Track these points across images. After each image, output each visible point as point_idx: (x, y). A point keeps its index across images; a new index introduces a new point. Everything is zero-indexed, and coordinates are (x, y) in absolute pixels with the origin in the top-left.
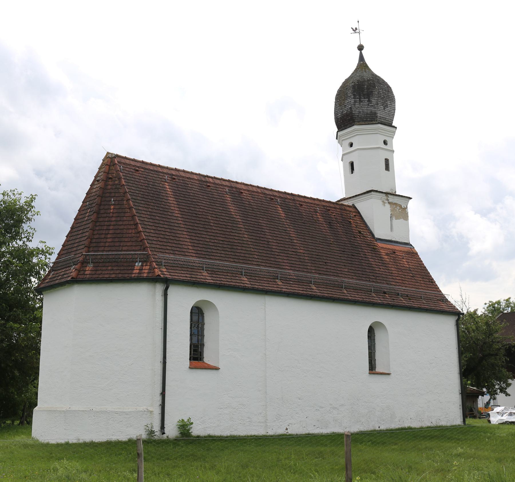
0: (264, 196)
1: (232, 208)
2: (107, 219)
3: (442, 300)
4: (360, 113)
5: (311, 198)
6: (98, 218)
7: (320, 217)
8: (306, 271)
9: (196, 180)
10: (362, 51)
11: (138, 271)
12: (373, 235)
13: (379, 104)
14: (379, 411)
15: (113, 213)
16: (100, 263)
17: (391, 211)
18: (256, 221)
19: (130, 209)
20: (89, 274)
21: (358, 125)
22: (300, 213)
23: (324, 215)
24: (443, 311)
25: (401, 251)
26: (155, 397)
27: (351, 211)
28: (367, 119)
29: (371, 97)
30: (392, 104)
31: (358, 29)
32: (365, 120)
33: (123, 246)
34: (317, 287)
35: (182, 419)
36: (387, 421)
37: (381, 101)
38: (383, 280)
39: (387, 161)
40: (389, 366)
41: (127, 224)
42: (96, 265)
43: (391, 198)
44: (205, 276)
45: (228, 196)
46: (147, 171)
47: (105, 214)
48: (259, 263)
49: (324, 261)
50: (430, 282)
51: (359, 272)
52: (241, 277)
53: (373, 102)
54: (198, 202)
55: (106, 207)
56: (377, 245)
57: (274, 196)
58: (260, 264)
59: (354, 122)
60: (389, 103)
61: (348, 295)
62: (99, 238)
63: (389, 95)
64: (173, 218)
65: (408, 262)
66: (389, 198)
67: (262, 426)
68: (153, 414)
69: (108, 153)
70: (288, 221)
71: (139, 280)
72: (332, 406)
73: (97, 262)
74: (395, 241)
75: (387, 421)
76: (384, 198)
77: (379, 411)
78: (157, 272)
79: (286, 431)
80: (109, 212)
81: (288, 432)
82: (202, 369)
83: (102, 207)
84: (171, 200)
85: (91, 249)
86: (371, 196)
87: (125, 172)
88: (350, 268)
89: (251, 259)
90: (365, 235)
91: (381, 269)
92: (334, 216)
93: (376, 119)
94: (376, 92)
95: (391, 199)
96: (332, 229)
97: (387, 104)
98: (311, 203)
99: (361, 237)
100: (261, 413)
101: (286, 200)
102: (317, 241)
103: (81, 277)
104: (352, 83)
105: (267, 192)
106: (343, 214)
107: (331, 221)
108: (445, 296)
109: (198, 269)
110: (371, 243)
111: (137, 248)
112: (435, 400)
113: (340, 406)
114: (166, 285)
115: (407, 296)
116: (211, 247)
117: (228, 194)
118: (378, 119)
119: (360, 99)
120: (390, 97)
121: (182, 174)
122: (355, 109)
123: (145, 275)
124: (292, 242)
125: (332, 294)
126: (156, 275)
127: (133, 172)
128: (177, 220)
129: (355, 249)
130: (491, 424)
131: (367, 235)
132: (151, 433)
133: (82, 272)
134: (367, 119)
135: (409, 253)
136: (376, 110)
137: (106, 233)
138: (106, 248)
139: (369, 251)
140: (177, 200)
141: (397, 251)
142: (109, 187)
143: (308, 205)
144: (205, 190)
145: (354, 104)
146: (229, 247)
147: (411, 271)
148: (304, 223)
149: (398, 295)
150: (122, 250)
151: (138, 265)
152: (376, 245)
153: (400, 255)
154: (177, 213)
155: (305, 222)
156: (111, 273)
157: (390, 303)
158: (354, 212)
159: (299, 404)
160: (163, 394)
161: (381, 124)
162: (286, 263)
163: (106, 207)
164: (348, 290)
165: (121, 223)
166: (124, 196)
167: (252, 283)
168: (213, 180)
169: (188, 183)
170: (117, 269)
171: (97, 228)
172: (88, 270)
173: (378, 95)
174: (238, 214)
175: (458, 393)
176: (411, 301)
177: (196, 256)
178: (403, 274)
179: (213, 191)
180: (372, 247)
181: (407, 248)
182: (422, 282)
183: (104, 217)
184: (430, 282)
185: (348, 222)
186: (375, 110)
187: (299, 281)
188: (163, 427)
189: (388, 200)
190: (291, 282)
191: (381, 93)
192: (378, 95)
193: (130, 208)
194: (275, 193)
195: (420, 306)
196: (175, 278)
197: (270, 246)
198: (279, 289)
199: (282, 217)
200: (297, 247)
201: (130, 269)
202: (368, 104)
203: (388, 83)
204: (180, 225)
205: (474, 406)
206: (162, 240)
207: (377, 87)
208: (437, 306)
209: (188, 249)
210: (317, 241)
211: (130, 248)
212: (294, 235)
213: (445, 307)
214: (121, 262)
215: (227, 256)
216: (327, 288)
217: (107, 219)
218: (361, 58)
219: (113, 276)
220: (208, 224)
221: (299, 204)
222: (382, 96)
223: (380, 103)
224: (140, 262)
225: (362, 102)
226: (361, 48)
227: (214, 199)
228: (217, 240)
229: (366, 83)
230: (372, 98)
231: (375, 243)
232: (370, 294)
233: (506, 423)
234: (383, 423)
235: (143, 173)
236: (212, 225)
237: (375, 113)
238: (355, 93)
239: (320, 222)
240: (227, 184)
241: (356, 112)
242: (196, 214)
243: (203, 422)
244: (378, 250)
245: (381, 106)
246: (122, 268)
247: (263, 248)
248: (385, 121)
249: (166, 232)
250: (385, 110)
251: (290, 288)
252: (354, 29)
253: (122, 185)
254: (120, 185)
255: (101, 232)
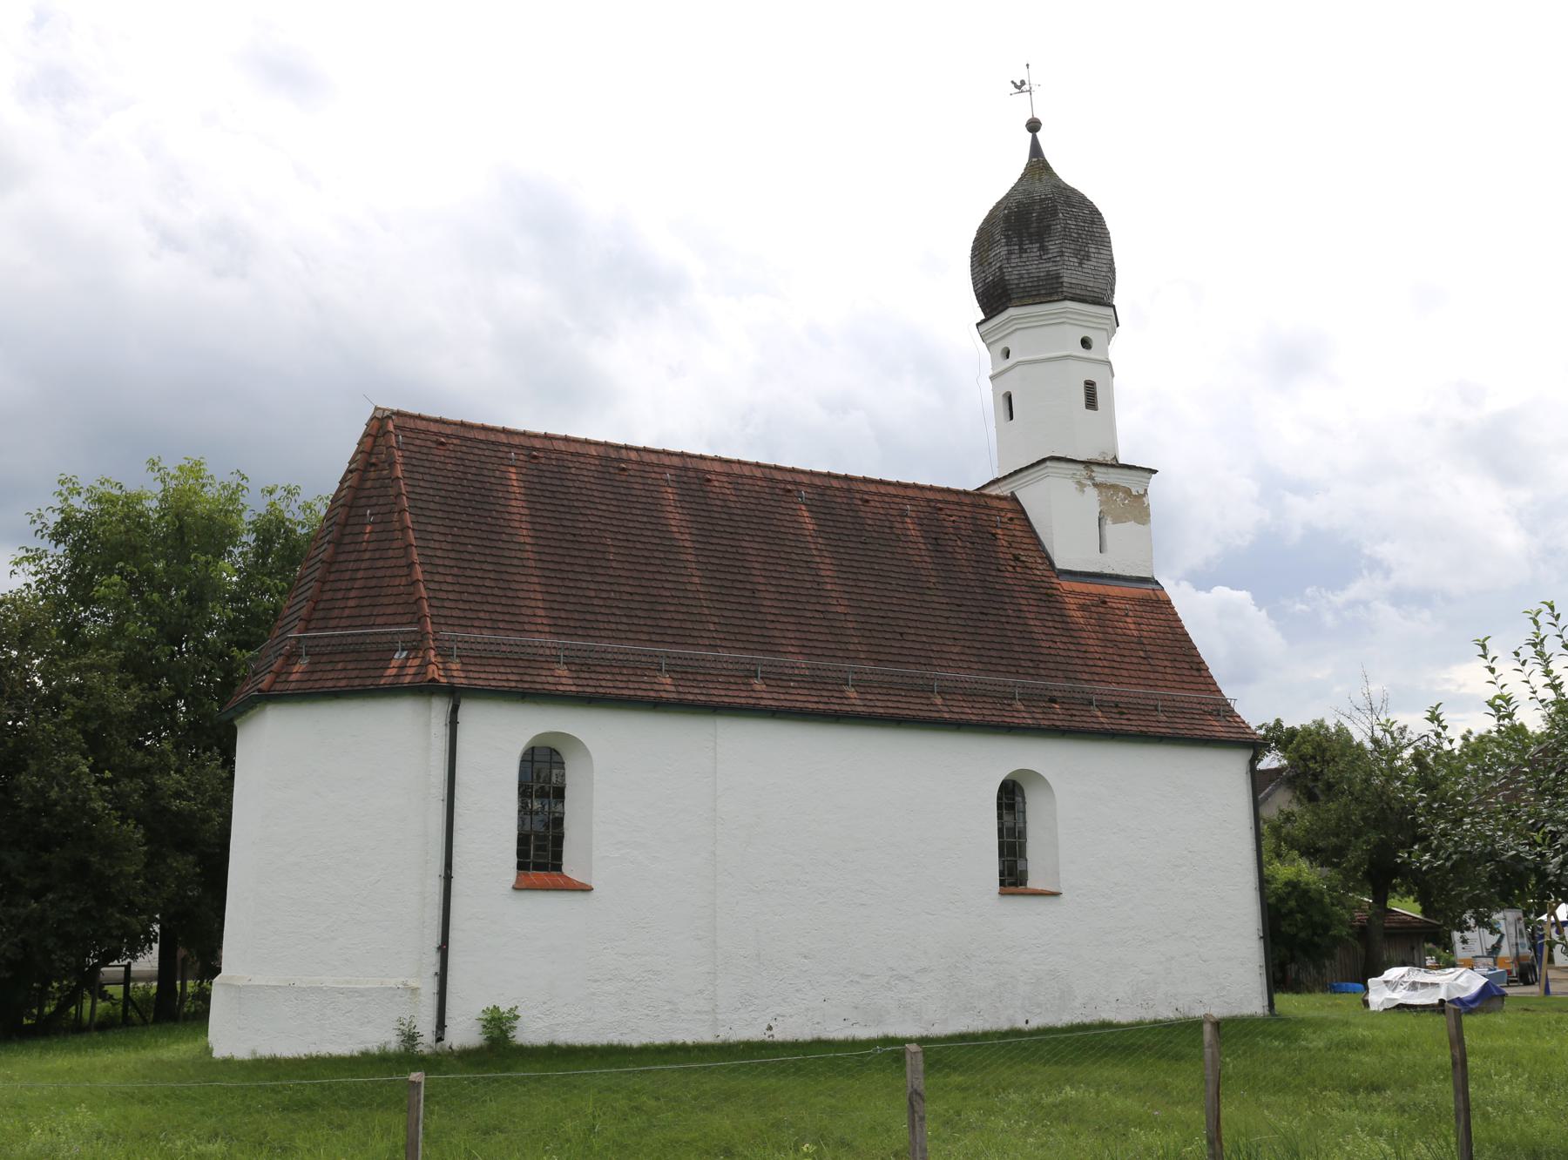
0: (770, 484)
1: (675, 519)
2: (353, 556)
3: (1215, 713)
4: (1022, 278)
5: (898, 484)
6: (336, 553)
7: (911, 527)
8: (841, 655)
9: (593, 456)
10: (1038, 134)
11: (394, 671)
12: (1052, 564)
13: (1066, 254)
14: (1025, 984)
15: (368, 542)
16: (323, 654)
17: (1102, 503)
18: (732, 543)
19: (402, 530)
20: (297, 681)
21: (1041, 303)
22: (859, 520)
23: (925, 522)
24: (1208, 740)
25: (1123, 598)
26: (424, 956)
27: (1002, 510)
28: (1039, 290)
29: (1047, 240)
30: (1102, 251)
31: (1027, 82)
32: (1034, 293)
33: (377, 615)
34: (861, 693)
35: (494, 1006)
36: (1049, 1006)
37: (1073, 246)
38: (1057, 670)
39: (1090, 388)
40: (1058, 874)
41: (393, 565)
42: (316, 659)
43: (1101, 473)
44: (562, 676)
45: (669, 490)
46: (469, 443)
47: (353, 545)
48: (718, 640)
49: (897, 629)
50: (1192, 668)
51: (993, 653)
52: (656, 677)
53: (1051, 251)
54: (585, 507)
55: (357, 529)
56: (1059, 587)
57: (795, 483)
58: (719, 643)
59: (1010, 300)
60: (1094, 250)
61: (945, 709)
62: (333, 599)
63: (1095, 230)
64: (512, 546)
65: (1139, 624)
66: (1093, 474)
67: (705, 1022)
68: (420, 994)
69: (377, 409)
70: (820, 540)
71: (394, 691)
72: (895, 973)
73: (318, 654)
74: (1110, 574)
75: (1049, 1006)
76: (1081, 475)
77: (1025, 984)
78: (434, 672)
79: (769, 1033)
80: (360, 540)
81: (773, 1036)
82: (548, 890)
83: (348, 529)
84: (517, 505)
85: (313, 625)
86: (1046, 471)
87: (411, 447)
88: (968, 644)
89: (696, 633)
90: (1029, 565)
91: (1056, 642)
92: (954, 521)
93: (1060, 290)
94: (1059, 226)
95: (1101, 475)
96: (938, 554)
97: (1088, 252)
98: (895, 496)
99: (1018, 569)
100: (701, 992)
101: (828, 492)
102: (890, 584)
103: (278, 687)
104: (1005, 209)
105: (778, 476)
106: (979, 516)
107: (942, 536)
108: (1229, 701)
109: (547, 661)
110: (1043, 581)
111: (404, 619)
112: (1187, 955)
113: (917, 972)
114: (452, 701)
115: (1117, 706)
116: (597, 610)
117: (671, 484)
118: (1065, 289)
119: (1021, 244)
120: (1097, 235)
121: (561, 446)
122: (1010, 270)
123: (407, 679)
124: (819, 590)
125: (898, 708)
126: (427, 680)
127: (430, 448)
128: (520, 550)
129: (994, 598)
130: (1366, 1010)
131: (1036, 562)
132: (411, 1037)
133: (283, 677)
134: (1039, 290)
135: (1147, 601)
136: (1058, 268)
137: (349, 587)
138: (343, 620)
139: (1032, 602)
140: (531, 505)
141: (1113, 597)
142: (369, 484)
143: (886, 499)
144: (610, 480)
145: (1007, 259)
146: (646, 606)
147: (1144, 644)
148: (866, 543)
149: (1091, 703)
150: (374, 625)
151: (400, 656)
152: (1054, 586)
153: (1118, 609)
154: (524, 535)
155: (868, 541)
156: (340, 677)
157: (1058, 723)
158: (1010, 511)
159: (804, 969)
160: (443, 949)
161: (1072, 299)
162: (791, 638)
163: (357, 529)
164: (947, 697)
165: (380, 564)
166: (395, 504)
167: (681, 689)
168: (640, 456)
169: (571, 465)
170: (354, 667)
171: (332, 577)
172: (297, 672)
173: (1063, 233)
174: (687, 531)
175: (1256, 937)
176: (1125, 717)
177: (550, 632)
178: (1119, 652)
179: (632, 480)
180: (1044, 591)
181: (1144, 591)
182: (1168, 670)
183: (349, 552)
184: (1192, 668)
185: (990, 536)
186: (1055, 268)
187: (815, 681)
188: (441, 1025)
189: (1093, 479)
190: (792, 684)
191: (1073, 227)
192: (1063, 233)
193: (404, 529)
194: (801, 475)
195: (1144, 729)
196: (476, 685)
197: (756, 602)
198: (753, 701)
199: (807, 533)
200: (830, 601)
201: (381, 668)
202: (1041, 255)
203: (1095, 203)
204: (525, 563)
205: (1414, 958)
206: (471, 598)
207: (1061, 215)
208: (1197, 727)
209: (535, 615)
210: (890, 584)
211: (391, 620)
212: (829, 573)
213: (1218, 729)
214: (366, 651)
215: (634, 628)
216: (889, 694)
217: (353, 556)
218: (1036, 150)
219: (343, 683)
220: (599, 555)
221: (861, 499)
222: (1073, 234)
223: (1069, 251)
224: (403, 650)
225: (1026, 252)
226: (1034, 126)
227: (630, 498)
228: (614, 591)
229: (1036, 207)
230: (1048, 241)
231: (1055, 581)
232: (1009, 705)
233: (1401, 1007)
234: (1038, 1011)
235: (458, 448)
236: (611, 558)
237: (1058, 277)
238: (1010, 233)
239: (911, 539)
240: (676, 461)
241: (1013, 277)
242: (574, 535)
243: (548, 1013)
244: (1060, 599)
245: (1070, 259)
246: (365, 665)
247: (735, 606)
248: (1084, 293)
249: (486, 578)
250: (1084, 266)
251: (782, 697)
252: (1019, 84)
253: (394, 479)
254: (390, 478)
255: (339, 585)
